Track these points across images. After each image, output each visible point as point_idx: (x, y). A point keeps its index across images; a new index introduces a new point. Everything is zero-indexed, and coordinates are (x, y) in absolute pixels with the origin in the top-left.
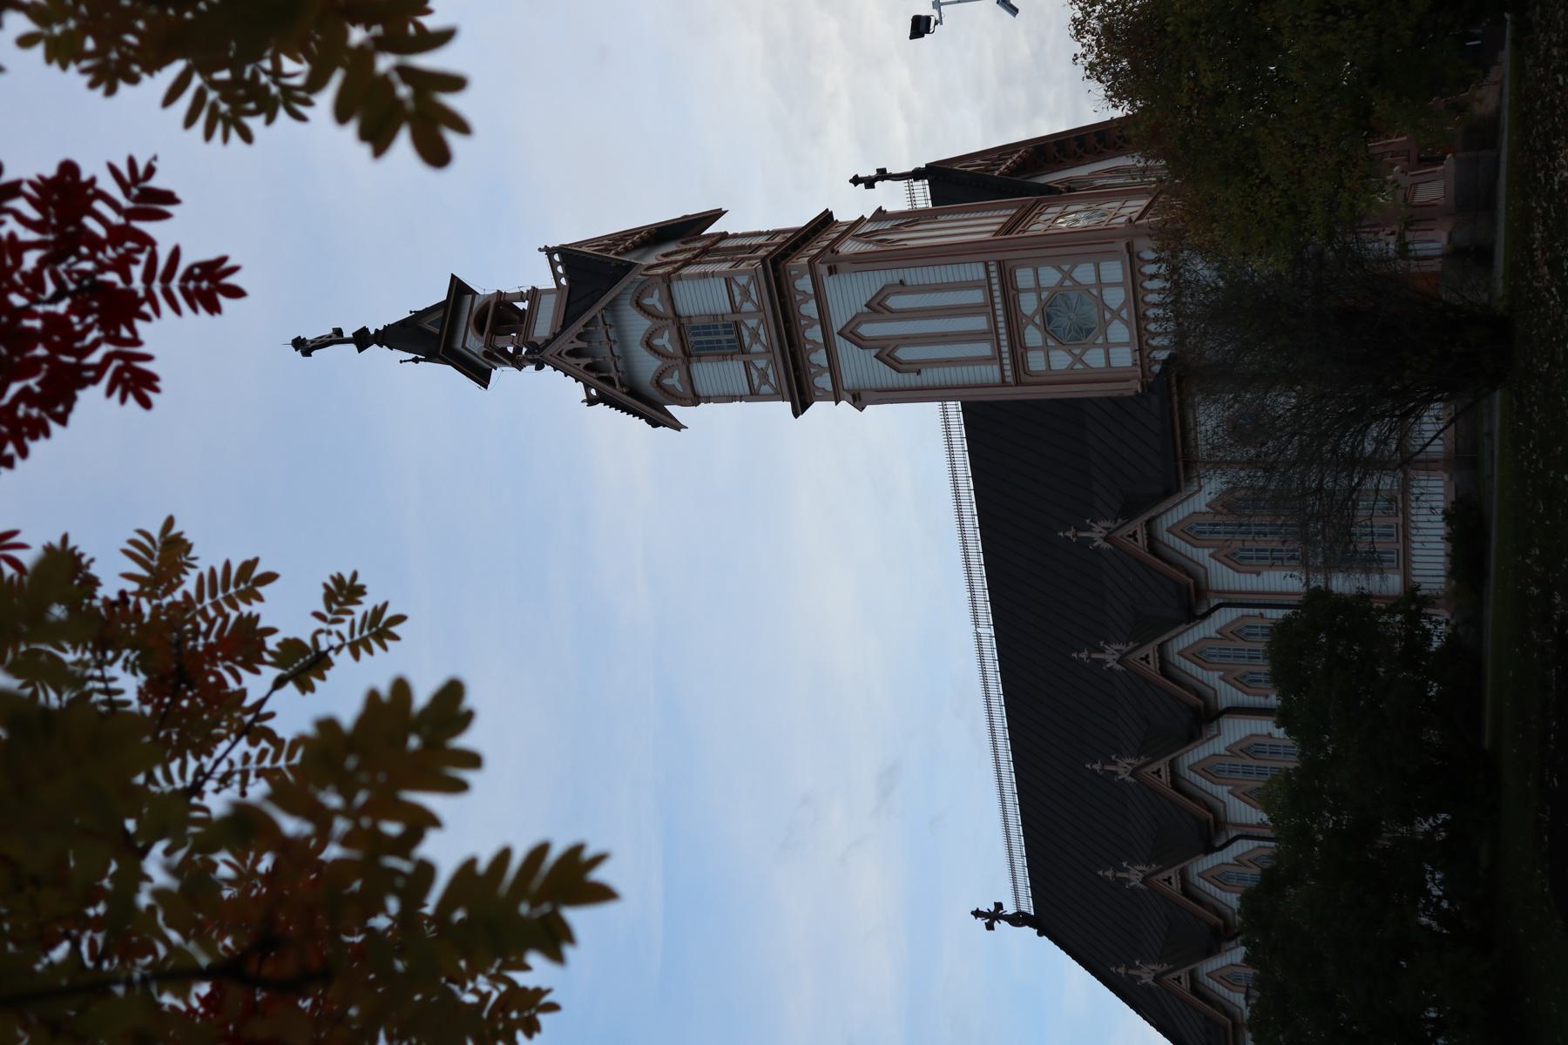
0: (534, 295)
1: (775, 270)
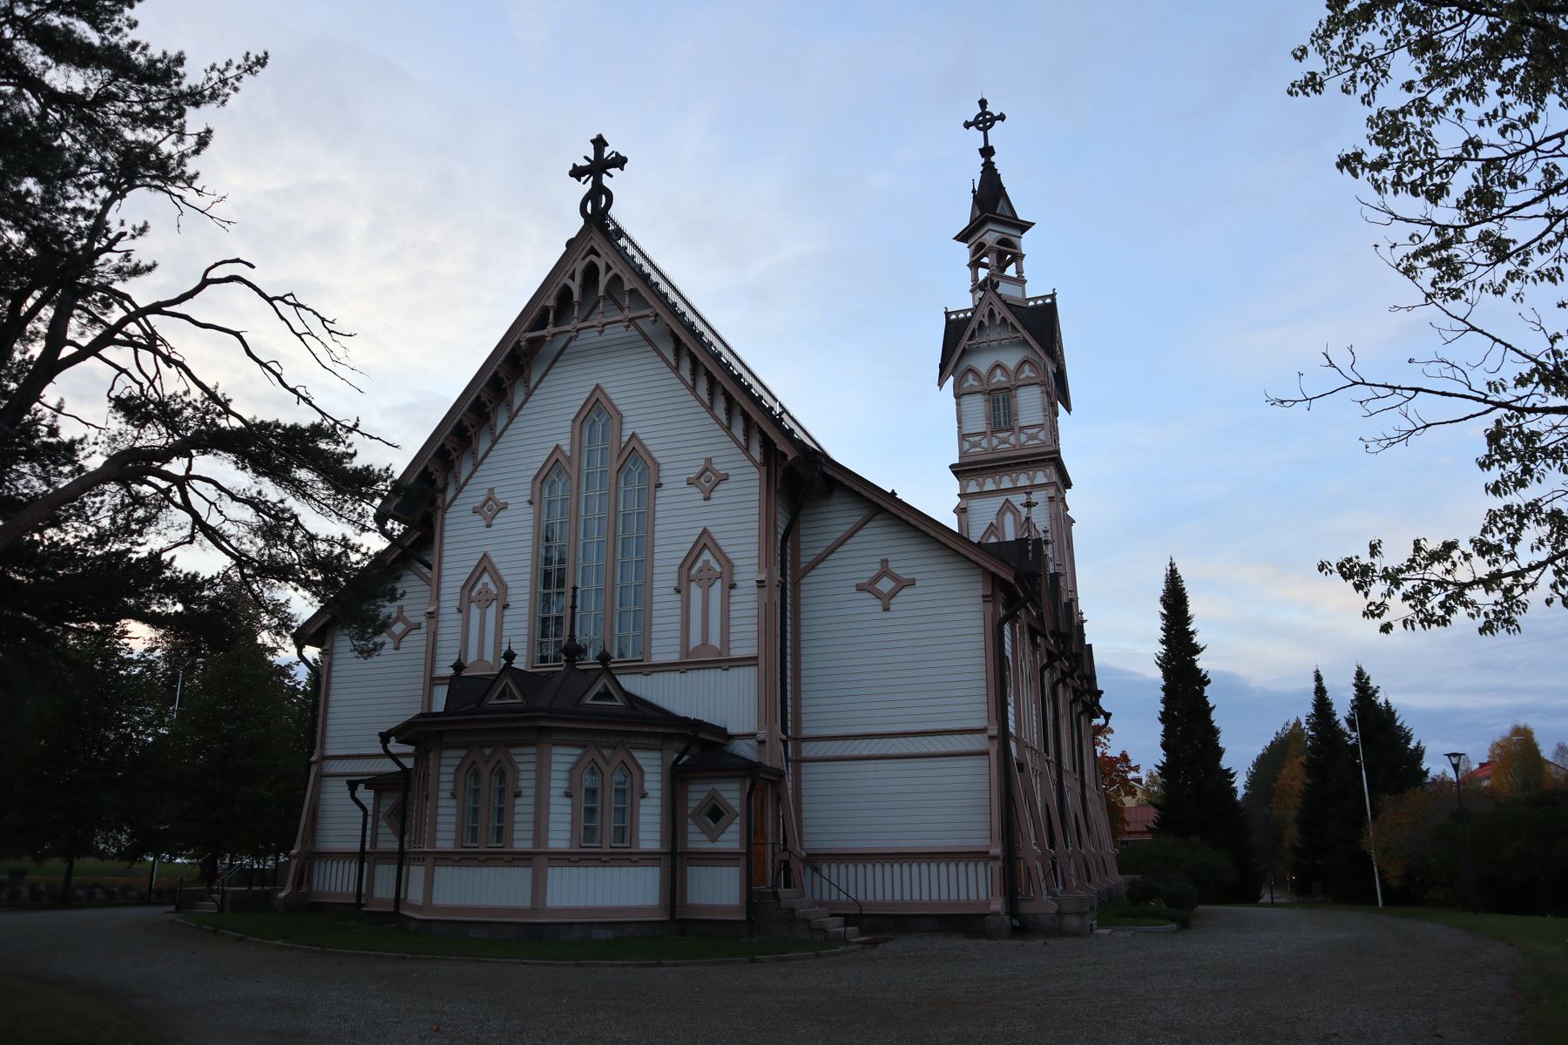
0: (1020, 281)
1: (1050, 459)
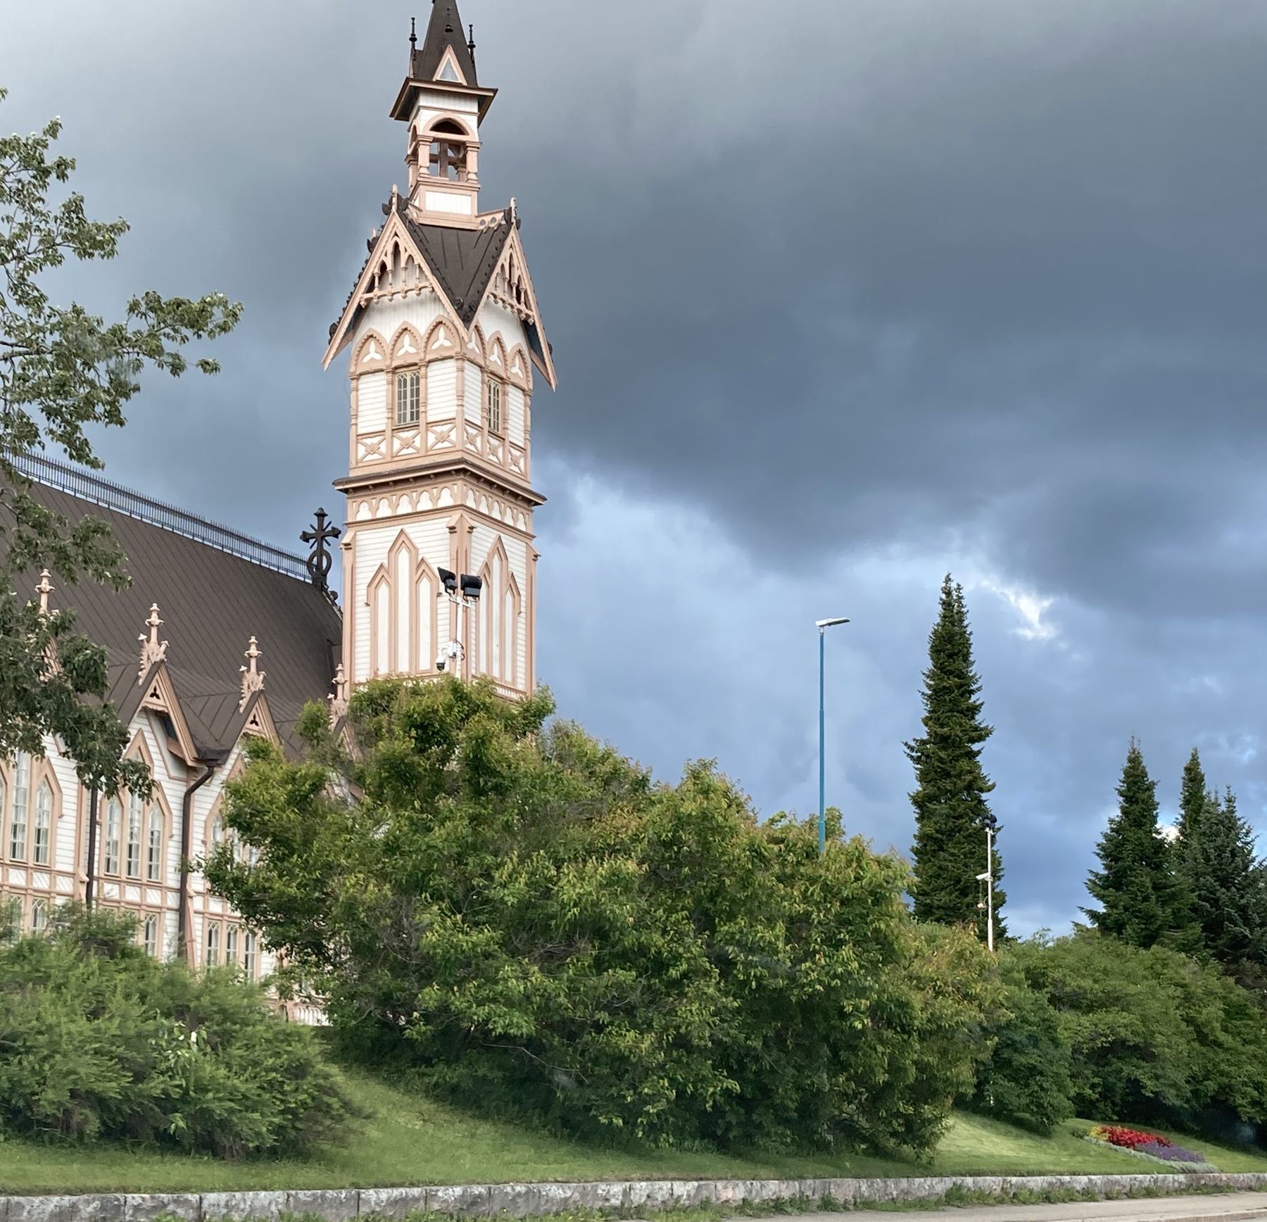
1: (458, 471)
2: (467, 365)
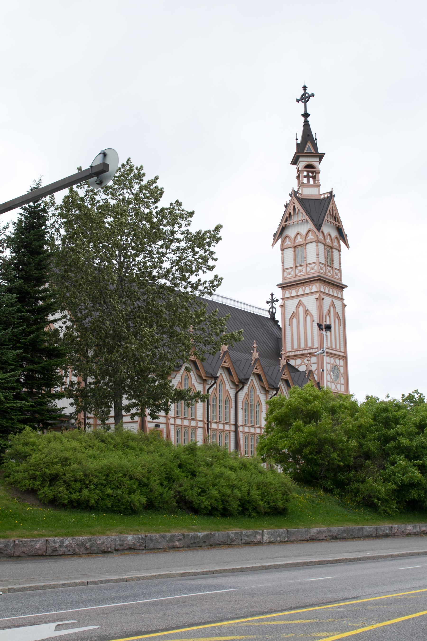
1: (318, 280)
2: (319, 244)
